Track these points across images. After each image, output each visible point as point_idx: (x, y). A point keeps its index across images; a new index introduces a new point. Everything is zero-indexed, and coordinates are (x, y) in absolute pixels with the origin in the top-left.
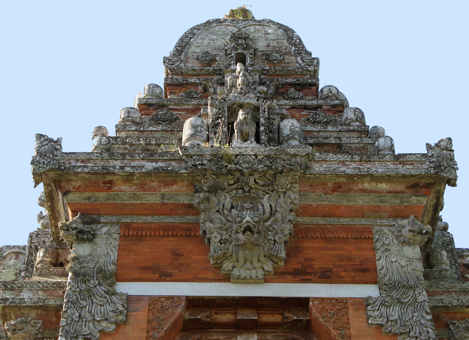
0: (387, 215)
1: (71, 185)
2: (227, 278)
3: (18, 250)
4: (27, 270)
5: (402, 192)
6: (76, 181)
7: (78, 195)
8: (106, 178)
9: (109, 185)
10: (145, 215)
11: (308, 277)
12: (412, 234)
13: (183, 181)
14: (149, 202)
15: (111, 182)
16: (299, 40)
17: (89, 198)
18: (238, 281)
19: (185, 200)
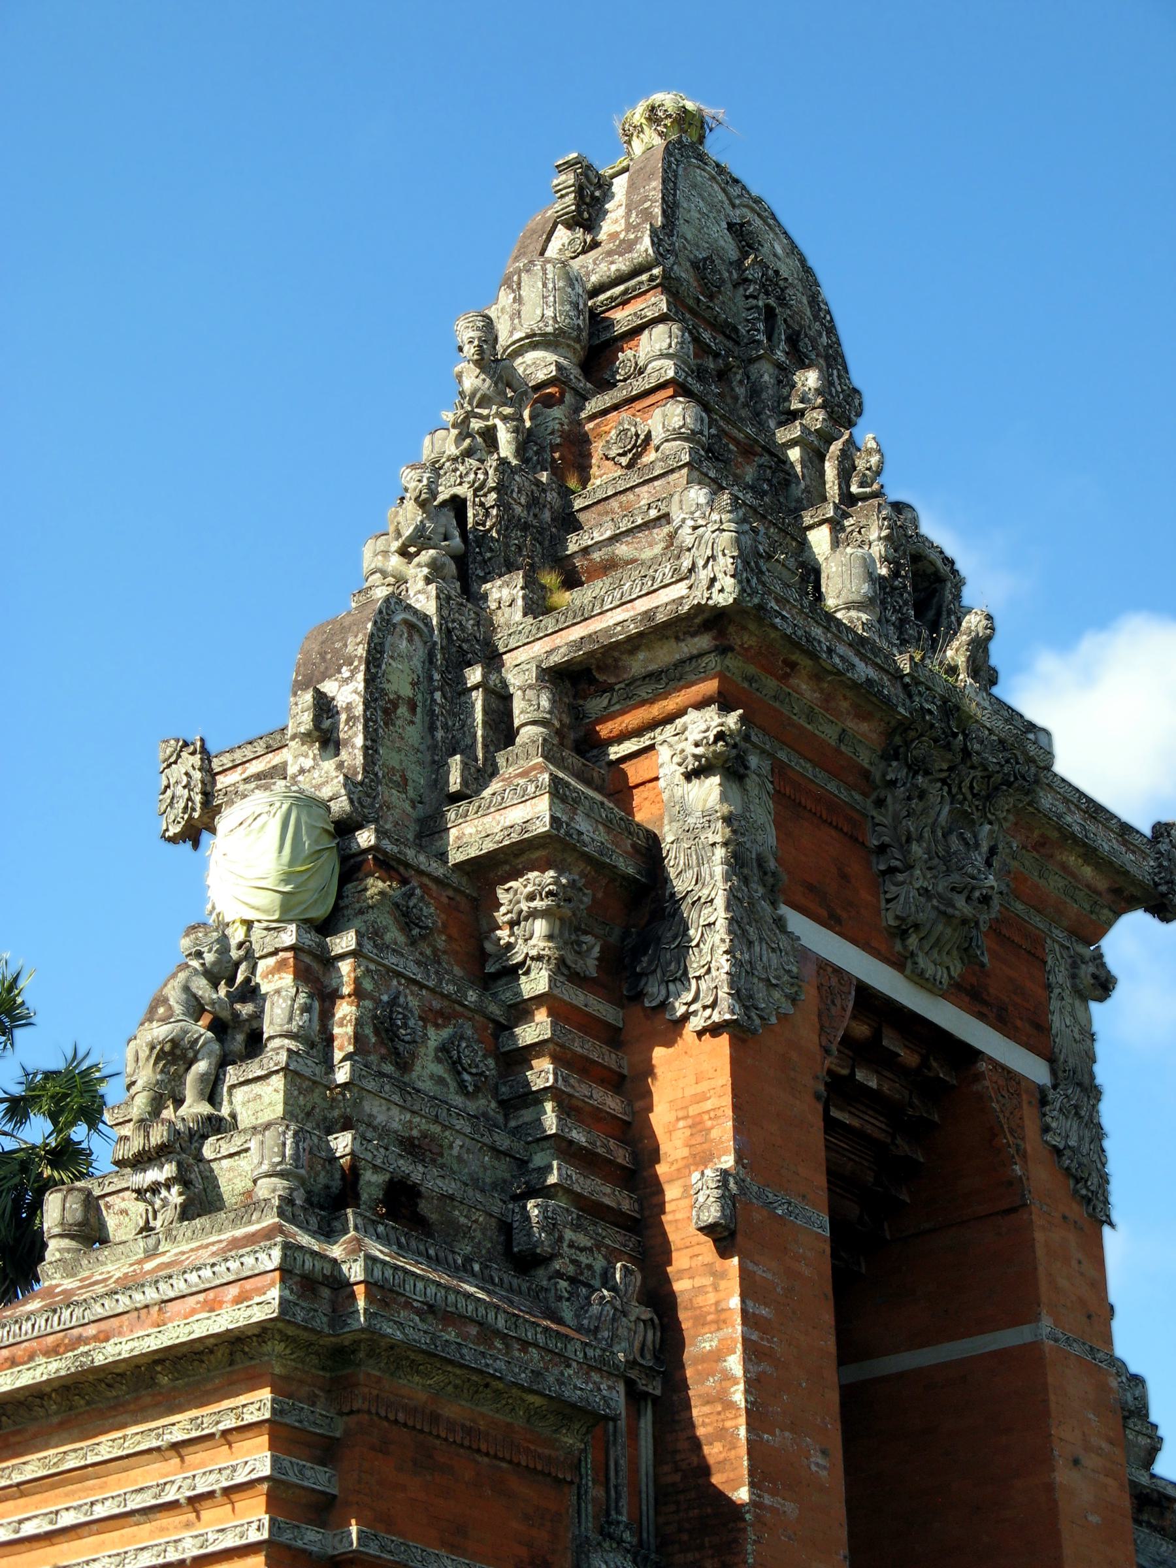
0: (1065, 923)
1: (741, 638)
2: (898, 963)
3: (414, 620)
4: (1077, 1181)
5: (1099, 894)
6: (751, 633)
7: (740, 664)
8: (793, 653)
9: (788, 670)
10: (805, 758)
11: (984, 1010)
12: (1092, 981)
13: (881, 720)
14: (823, 736)
15: (793, 666)
16: (768, 471)
17: (750, 680)
18: (916, 979)
19: (864, 759)
